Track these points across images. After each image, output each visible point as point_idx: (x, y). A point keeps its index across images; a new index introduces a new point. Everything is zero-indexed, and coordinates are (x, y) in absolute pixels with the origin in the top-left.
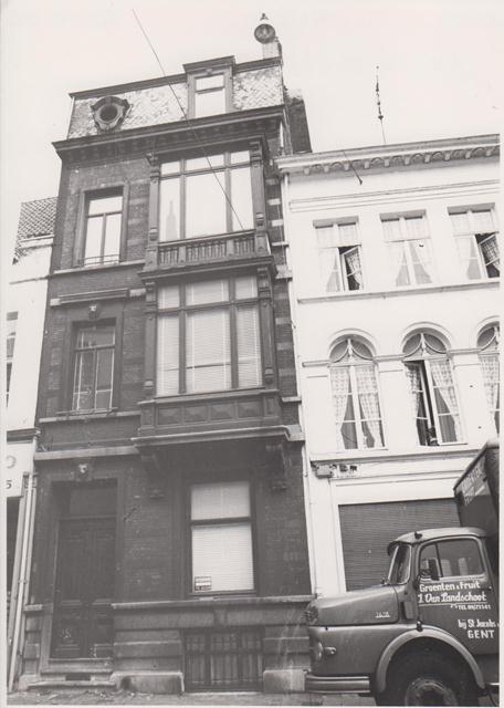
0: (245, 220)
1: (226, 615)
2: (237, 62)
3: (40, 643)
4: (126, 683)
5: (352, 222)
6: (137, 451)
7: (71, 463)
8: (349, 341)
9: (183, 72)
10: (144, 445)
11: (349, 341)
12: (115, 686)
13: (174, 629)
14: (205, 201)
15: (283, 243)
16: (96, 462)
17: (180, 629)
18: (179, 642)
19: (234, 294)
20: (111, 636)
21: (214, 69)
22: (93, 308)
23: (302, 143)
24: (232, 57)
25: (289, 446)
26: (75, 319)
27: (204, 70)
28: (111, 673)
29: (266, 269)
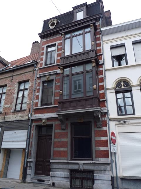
0: (88, 47)
1: (107, 89)
2: (88, 4)
3: (31, 170)
4: (53, 184)
5: (123, 45)
6: (57, 116)
7: (40, 120)
8: (122, 81)
9: (72, 10)
10: (105, 94)
11: (122, 81)
12: (50, 185)
13: (67, 169)
14: (77, 44)
15: (101, 53)
16: (48, 119)
17: (69, 169)
18: (68, 173)
19: (85, 69)
20: (50, 170)
21: (81, 7)
22: (47, 77)
23: (108, 22)
24: (86, 3)
25: (103, 114)
26: (43, 80)
27: (78, 8)
28: (49, 181)
29: (94, 60)
